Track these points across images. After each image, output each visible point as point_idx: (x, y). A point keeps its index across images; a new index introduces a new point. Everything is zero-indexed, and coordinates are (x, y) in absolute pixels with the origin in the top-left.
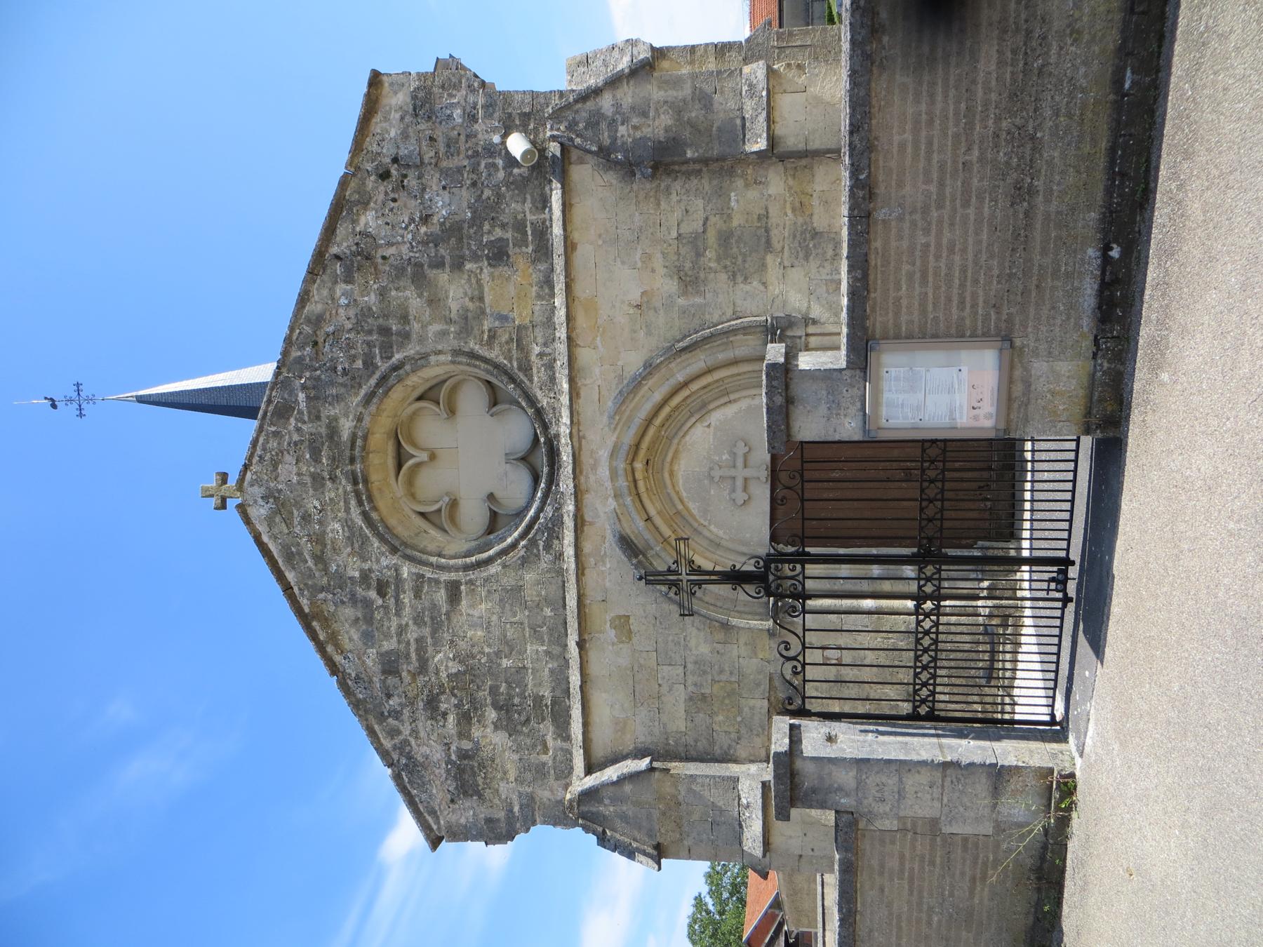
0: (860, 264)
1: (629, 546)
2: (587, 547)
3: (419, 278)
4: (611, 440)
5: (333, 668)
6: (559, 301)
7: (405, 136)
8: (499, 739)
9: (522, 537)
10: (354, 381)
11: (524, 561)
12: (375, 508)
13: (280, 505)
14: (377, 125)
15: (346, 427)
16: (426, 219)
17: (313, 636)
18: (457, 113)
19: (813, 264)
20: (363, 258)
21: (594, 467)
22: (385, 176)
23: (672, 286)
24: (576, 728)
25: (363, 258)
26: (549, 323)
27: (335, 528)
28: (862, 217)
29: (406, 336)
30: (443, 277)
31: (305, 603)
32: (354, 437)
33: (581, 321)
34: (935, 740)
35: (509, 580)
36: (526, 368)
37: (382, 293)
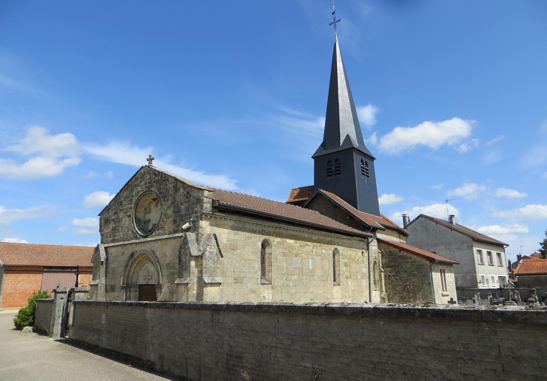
0: (123, 304)
1: (132, 255)
2: (134, 245)
3: (173, 203)
4: (147, 249)
5: (121, 191)
6: (167, 236)
7: (194, 197)
8: (111, 228)
9: (136, 231)
10: (159, 190)
11: (133, 231)
12: (142, 197)
13: (143, 175)
14: (196, 190)
15: (153, 189)
16: (181, 203)
17: (125, 186)
18: (196, 209)
19: (168, 294)
20: (176, 189)
21: (144, 246)
22: (188, 193)
23: (168, 262)
24: (112, 244)
25: (176, 189)
26: (165, 234)
27: (139, 189)
28: (131, 304)
29: (164, 202)
30: (172, 209)
31: (130, 183)
32: (151, 191)
33: (164, 241)
34: (61, 315)
35: (130, 228)
36: (158, 230)
37: (171, 195)
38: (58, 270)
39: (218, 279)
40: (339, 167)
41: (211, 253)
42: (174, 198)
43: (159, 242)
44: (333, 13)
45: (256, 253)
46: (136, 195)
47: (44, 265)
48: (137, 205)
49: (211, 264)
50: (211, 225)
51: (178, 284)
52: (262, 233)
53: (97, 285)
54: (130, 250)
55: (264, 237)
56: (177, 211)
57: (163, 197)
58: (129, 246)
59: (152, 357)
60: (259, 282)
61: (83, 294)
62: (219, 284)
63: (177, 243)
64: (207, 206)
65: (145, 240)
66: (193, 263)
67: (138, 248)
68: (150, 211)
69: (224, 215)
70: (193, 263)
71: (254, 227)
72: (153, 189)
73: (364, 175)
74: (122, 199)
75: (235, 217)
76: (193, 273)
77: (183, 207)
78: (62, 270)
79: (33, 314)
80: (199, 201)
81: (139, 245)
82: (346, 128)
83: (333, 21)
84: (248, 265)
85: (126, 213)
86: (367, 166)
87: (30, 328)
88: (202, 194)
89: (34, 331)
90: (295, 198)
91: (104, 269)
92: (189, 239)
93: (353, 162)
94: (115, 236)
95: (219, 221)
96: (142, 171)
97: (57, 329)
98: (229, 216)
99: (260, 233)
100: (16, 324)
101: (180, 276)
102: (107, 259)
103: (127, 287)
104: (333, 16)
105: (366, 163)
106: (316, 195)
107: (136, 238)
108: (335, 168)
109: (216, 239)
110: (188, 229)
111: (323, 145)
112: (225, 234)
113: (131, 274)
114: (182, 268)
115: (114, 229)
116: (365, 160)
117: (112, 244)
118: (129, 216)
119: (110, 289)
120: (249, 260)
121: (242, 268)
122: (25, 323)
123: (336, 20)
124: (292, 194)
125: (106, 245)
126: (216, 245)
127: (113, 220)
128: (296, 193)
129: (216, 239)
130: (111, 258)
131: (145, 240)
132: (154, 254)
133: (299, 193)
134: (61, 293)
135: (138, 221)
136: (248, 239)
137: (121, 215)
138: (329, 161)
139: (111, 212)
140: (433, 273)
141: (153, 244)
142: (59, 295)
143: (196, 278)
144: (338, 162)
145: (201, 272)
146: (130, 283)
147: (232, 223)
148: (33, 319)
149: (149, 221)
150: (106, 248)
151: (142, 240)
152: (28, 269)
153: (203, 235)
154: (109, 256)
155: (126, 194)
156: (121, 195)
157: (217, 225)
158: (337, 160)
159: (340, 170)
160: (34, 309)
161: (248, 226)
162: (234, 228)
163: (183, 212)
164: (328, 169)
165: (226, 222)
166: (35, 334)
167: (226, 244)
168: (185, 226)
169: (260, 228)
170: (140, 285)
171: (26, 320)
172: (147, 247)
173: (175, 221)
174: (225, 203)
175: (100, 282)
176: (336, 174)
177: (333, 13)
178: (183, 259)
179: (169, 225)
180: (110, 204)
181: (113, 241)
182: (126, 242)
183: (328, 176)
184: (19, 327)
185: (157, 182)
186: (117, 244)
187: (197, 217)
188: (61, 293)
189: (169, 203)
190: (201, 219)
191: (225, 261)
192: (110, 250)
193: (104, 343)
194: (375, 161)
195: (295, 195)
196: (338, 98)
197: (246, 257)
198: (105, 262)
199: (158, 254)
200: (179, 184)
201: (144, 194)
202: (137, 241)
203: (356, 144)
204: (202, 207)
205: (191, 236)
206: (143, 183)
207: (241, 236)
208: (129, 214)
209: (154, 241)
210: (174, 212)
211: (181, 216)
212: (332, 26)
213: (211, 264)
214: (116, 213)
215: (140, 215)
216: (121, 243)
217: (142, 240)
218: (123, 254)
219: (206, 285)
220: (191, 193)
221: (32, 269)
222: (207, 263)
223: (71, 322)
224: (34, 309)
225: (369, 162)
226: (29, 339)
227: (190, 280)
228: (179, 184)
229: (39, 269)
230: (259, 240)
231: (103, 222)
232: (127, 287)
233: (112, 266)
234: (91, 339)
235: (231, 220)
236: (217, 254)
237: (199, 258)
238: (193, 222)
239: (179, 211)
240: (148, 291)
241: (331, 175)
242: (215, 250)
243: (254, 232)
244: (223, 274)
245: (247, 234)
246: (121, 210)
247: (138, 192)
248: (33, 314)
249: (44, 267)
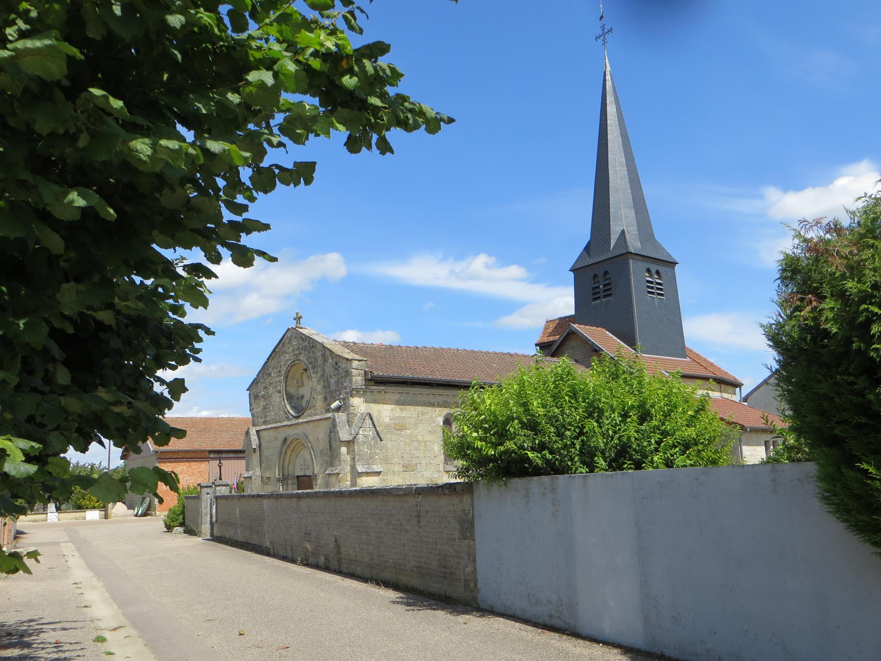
1: (285, 440)
3: (322, 376)
5: (268, 359)
6: (318, 417)
10: (308, 359)
25: (325, 360)
33: (316, 423)
38: (230, 455)
39: (376, 468)
40: (609, 284)
41: (366, 436)
42: (324, 370)
43: (311, 424)
44: (601, 18)
45: (435, 432)
46: (285, 365)
47: (210, 449)
48: (286, 378)
49: (366, 450)
50: (366, 401)
51: (329, 475)
52: (445, 405)
53: (250, 477)
54: (282, 434)
55: (445, 411)
56: (327, 386)
57: (314, 368)
58: (281, 430)
59: (267, 544)
60: (441, 468)
61: (224, 488)
62: (379, 473)
63: (326, 425)
64: (358, 380)
65: (297, 421)
66: (344, 450)
67: (291, 432)
68: (303, 384)
69: (383, 388)
70: (344, 450)
71: (431, 399)
72: (301, 358)
73: (653, 293)
74: (271, 369)
75: (400, 389)
76: (344, 461)
77: (332, 381)
78: (235, 455)
79: (183, 513)
80: (348, 374)
81: (291, 428)
82: (622, 219)
83: (601, 32)
84: (422, 448)
85: (275, 387)
86: (660, 277)
87: (181, 529)
88: (351, 365)
89: (185, 532)
90: (550, 335)
91: (258, 458)
92: (337, 420)
93: (629, 275)
94: (266, 416)
95: (377, 396)
96: (289, 334)
97: (206, 528)
98: (390, 389)
99: (439, 406)
100: (166, 526)
101: (331, 464)
102: (260, 446)
103: (284, 479)
104: (601, 23)
105: (658, 272)
106: (568, 334)
107: (288, 419)
108: (604, 286)
109: (372, 419)
110: (338, 409)
111: (588, 249)
112: (386, 412)
113: (286, 463)
114: (331, 456)
115: (265, 408)
116: (653, 268)
117: (263, 427)
118: (279, 392)
119: (265, 481)
120: (425, 442)
121: (415, 452)
122: (175, 524)
123: (606, 31)
124: (546, 328)
125: (258, 428)
126: (371, 426)
127: (263, 396)
128: (552, 326)
129: (372, 419)
130: (264, 444)
131: (297, 421)
132: (307, 438)
133: (556, 327)
134: (206, 487)
135: (290, 397)
136: (423, 414)
137: (271, 390)
138: (595, 276)
139: (261, 386)
140: (744, 448)
141: (305, 426)
142: (204, 490)
143: (349, 467)
144: (608, 277)
145: (353, 459)
146: (286, 474)
147: (397, 397)
148: (184, 519)
149: (303, 397)
150: (257, 432)
151: (294, 421)
152: (188, 455)
153: (356, 415)
154: (262, 441)
155: (272, 363)
156: (269, 364)
157: (375, 402)
158: (606, 273)
159: (610, 289)
160: (184, 507)
161: (420, 398)
162: (398, 403)
163: (333, 387)
164: (594, 289)
165: (387, 396)
166: (185, 535)
167: (389, 424)
168: (333, 406)
169: (440, 399)
170: (298, 477)
171: (177, 520)
172: (299, 431)
173: (325, 399)
174: (381, 374)
175: (254, 473)
176: (605, 296)
177: (601, 18)
178: (333, 445)
179: (319, 403)
180: (258, 375)
181: (265, 423)
182: (278, 425)
183: (595, 299)
184: (169, 528)
185: (305, 348)
186: (268, 426)
187: (347, 393)
188: (206, 487)
189: (319, 374)
190: (352, 396)
191: (389, 445)
192: (262, 434)
193: (240, 538)
194: (677, 267)
195: (550, 331)
196: (608, 169)
197: (420, 438)
198: (258, 449)
199: (311, 438)
200: (328, 353)
201: (293, 365)
202: (289, 423)
203: (634, 244)
204: (351, 380)
205: (341, 417)
206: (290, 350)
207: (411, 412)
208: (279, 388)
209: (306, 422)
210: (324, 387)
211: (331, 392)
212: (600, 41)
213: (366, 450)
214: (265, 388)
215: (292, 390)
216: (273, 425)
217: (294, 421)
218: (276, 439)
219: (361, 474)
220: (339, 364)
221: (193, 455)
222: (361, 448)
223: (214, 519)
224: (184, 507)
225: (663, 270)
226: (179, 540)
227: (341, 470)
228: (328, 353)
229: (203, 455)
230: (439, 416)
231: (253, 397)
232: (284, 479)
233: (266, 453)
234: (229, 534)
235: (394, 392)
236: (374, 438)
237: (349, 443)
238: (344, 399)
239: (329, 387)
240: (305, 481)
241: (599, 298)
242: (371, 433)
243: (432, 405)
244: (386, 460)
245: (420, 408)
246: (270, 384)
247: (287, 361)
248: (183, 513)
249: (210, 452)
